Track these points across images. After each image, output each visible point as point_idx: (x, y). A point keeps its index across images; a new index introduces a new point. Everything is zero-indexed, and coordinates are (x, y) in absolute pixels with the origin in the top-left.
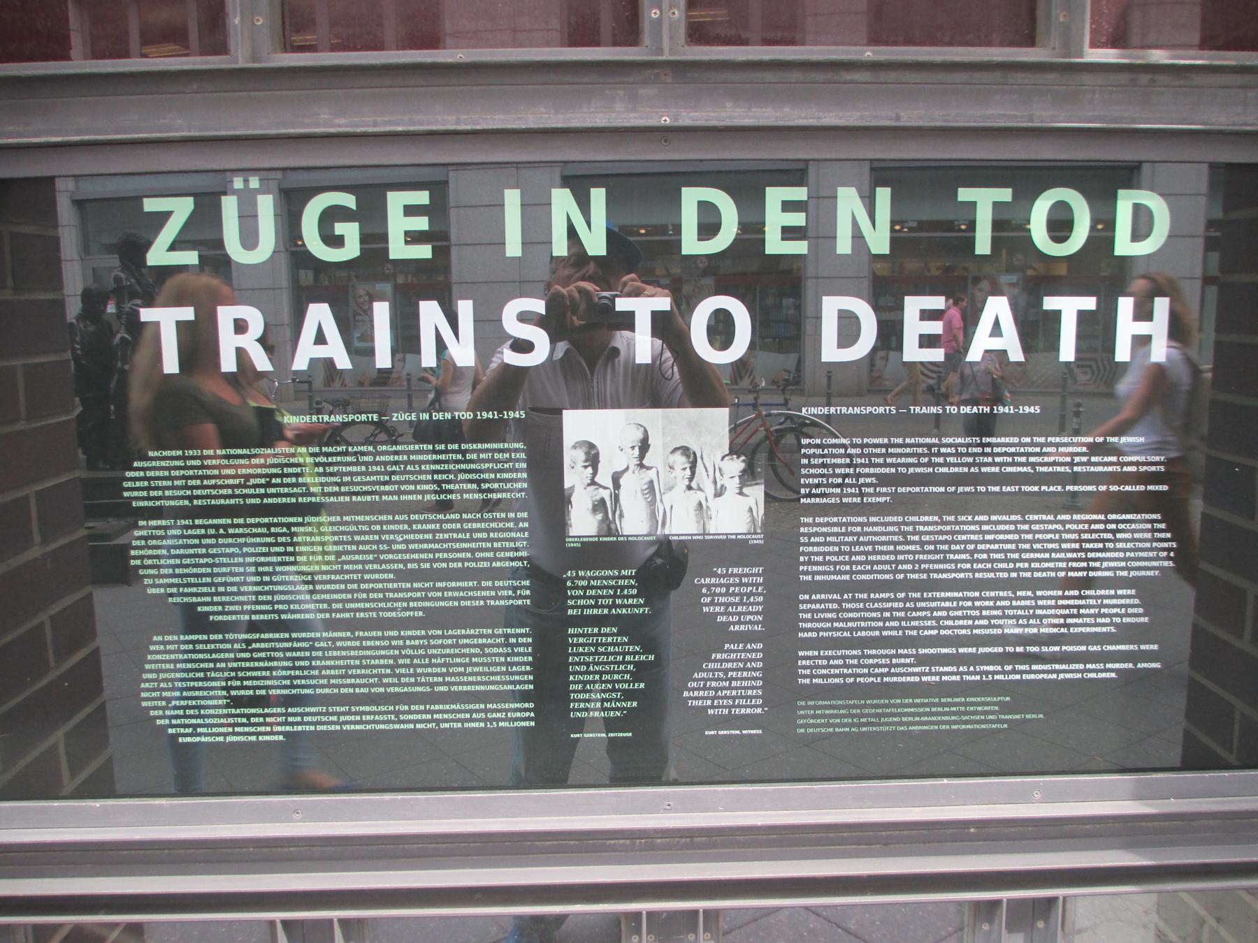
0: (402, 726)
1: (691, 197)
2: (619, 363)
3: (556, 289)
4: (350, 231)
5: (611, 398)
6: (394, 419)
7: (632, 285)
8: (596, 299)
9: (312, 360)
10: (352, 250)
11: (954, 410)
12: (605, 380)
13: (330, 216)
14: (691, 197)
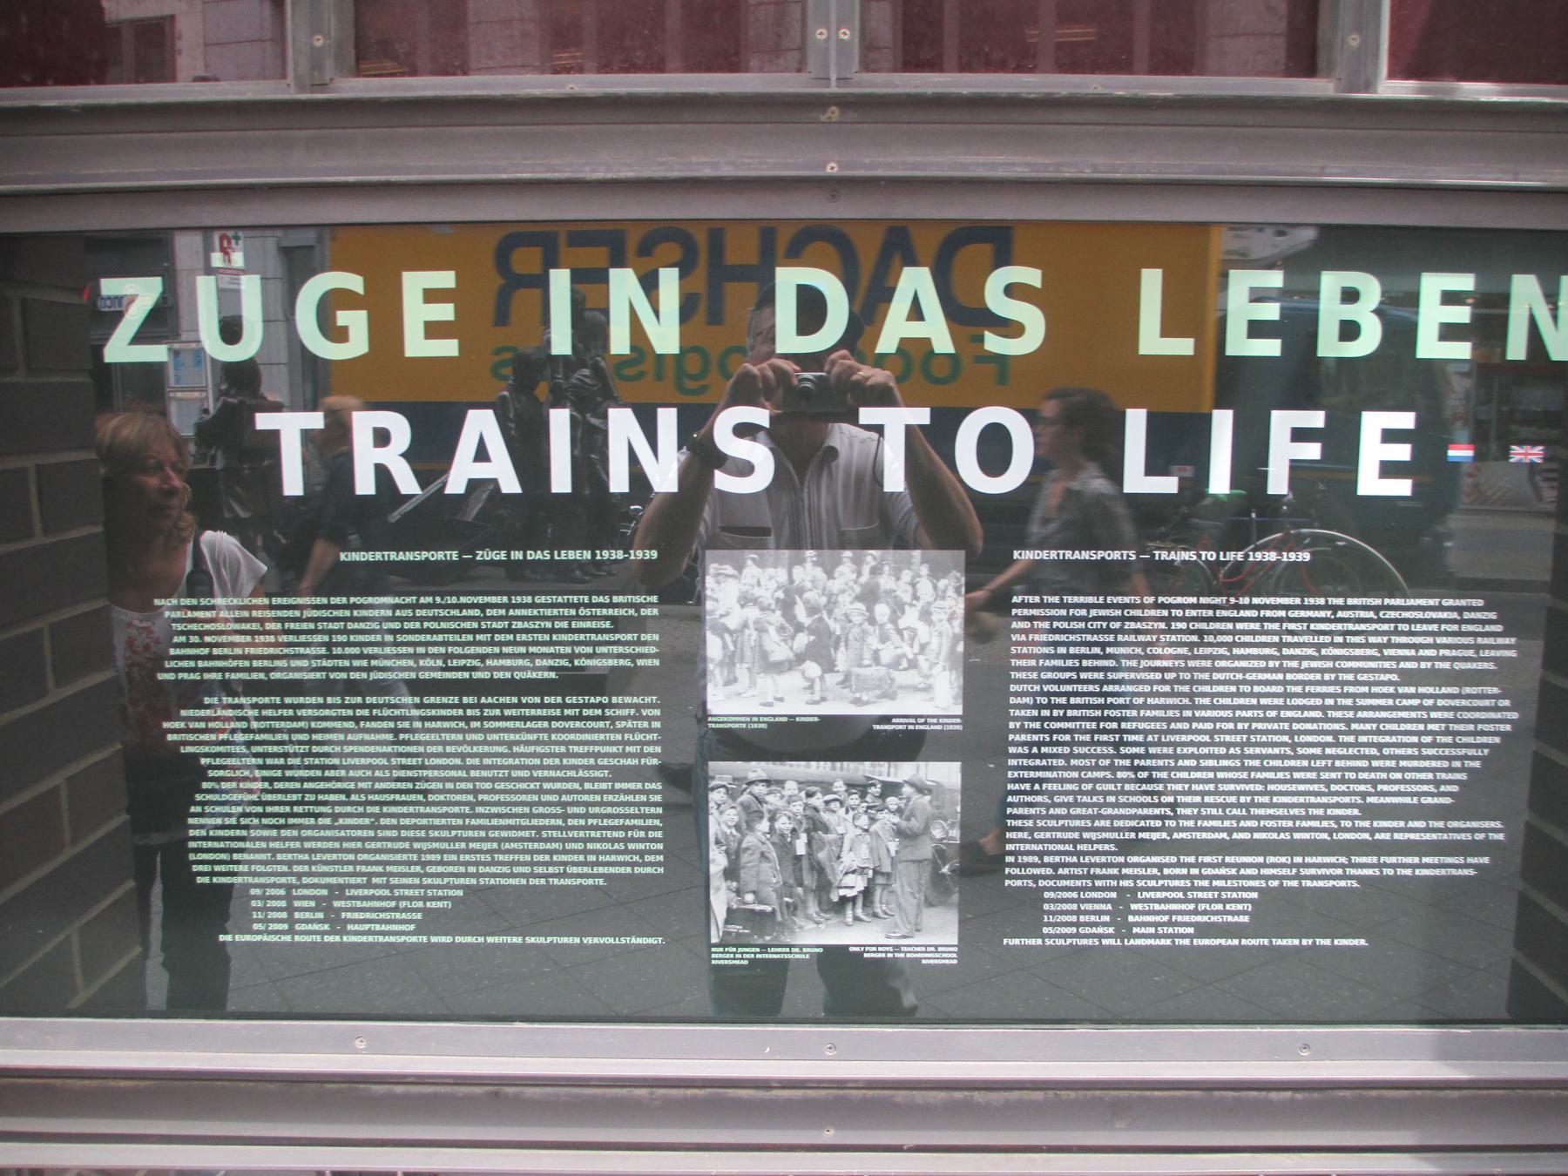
0: (1382, 800)
1: (788, 279)
2: (837, 466)
3: (745, 368)
4: (355, 321)
5: (827, 512)
6: (478, 558)
7: (842, 364)
8: (795, 382)
9: (902, 341)
10: (357, 345)
11: (1212, 556)
12: (819, 488)
13: (329, 305)
14: (788, 279)
